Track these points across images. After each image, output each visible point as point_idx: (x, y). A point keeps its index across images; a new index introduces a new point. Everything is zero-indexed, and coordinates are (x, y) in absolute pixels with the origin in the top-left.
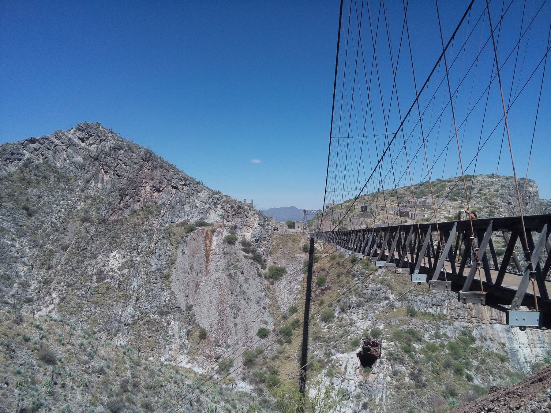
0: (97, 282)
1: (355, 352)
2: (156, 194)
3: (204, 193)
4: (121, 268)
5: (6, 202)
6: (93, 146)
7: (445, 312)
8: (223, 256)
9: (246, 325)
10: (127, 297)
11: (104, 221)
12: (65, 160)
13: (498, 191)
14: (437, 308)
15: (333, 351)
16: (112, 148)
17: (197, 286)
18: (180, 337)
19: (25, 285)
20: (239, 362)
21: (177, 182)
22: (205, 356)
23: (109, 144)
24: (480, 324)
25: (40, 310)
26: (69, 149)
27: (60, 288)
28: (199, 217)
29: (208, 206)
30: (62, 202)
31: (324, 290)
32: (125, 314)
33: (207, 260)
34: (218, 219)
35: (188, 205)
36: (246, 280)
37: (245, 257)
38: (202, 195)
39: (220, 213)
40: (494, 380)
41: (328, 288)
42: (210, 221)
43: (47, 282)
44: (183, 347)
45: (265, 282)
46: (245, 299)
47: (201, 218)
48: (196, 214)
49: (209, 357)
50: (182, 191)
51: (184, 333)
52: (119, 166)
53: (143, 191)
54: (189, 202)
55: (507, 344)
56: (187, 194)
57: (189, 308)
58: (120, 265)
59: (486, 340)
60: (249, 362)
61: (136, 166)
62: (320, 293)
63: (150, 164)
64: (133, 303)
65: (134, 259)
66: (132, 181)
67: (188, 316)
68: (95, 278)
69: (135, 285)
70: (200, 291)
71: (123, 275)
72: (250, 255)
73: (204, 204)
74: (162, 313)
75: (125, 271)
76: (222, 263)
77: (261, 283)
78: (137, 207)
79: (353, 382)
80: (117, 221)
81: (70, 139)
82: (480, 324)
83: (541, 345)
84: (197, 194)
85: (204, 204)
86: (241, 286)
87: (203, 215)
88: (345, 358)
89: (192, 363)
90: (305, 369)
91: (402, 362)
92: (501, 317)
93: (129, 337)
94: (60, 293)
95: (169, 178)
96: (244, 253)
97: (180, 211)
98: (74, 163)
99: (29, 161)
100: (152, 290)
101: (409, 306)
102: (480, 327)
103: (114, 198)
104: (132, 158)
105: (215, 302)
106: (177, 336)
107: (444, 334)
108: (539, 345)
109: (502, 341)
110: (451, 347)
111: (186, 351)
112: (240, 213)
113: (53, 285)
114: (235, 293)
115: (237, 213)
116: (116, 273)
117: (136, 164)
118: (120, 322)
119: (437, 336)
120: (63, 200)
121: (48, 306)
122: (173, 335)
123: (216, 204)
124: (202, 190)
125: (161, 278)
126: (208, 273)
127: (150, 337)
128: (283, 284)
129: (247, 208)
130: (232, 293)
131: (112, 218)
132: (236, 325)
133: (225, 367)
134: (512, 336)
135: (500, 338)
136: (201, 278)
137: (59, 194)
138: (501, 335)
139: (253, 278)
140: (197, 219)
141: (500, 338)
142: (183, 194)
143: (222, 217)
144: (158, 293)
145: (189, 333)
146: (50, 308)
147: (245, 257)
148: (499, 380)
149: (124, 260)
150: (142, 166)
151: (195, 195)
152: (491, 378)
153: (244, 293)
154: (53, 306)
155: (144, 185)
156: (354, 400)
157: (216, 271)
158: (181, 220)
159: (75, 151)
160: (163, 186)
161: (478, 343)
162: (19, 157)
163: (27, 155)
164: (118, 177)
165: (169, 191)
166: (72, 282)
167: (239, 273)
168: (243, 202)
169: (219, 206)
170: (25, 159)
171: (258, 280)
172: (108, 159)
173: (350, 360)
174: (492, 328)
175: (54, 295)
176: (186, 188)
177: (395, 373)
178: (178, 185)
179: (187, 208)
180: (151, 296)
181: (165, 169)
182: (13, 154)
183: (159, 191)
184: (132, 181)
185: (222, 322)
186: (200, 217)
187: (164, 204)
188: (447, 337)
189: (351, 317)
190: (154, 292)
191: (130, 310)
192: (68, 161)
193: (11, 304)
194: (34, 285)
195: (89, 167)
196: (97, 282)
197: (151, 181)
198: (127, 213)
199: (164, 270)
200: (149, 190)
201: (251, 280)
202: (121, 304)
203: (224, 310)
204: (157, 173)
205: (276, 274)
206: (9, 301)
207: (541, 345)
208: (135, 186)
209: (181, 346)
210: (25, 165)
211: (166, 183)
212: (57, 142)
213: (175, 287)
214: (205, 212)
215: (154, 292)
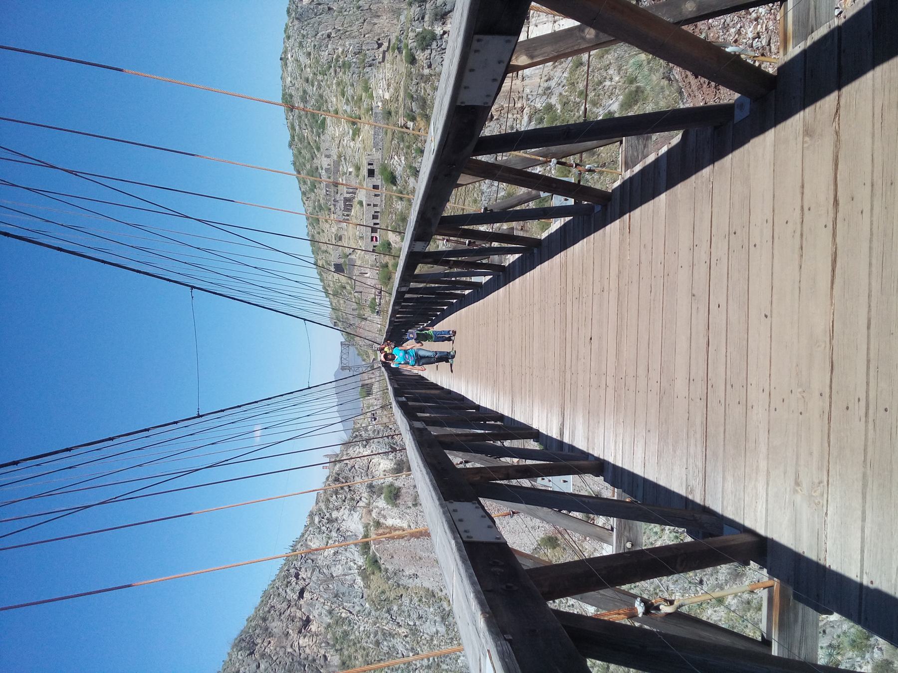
13: (309, 54)
24: (525, 96)
35: (333, 569)
39: (347, 512)
40: (611, 79)
48: (348, 554)
53: (308, 651)
54: (328, 567)
56: (313, 571)
59: (549, 88)
82: (525, 96)
102: (530, 97)
123: (330, 521)
148: (611, 72)
152: (607, 83)
161: (554, 100)
169: (335, 514)
179: (337, 571)
200: (306, 640)
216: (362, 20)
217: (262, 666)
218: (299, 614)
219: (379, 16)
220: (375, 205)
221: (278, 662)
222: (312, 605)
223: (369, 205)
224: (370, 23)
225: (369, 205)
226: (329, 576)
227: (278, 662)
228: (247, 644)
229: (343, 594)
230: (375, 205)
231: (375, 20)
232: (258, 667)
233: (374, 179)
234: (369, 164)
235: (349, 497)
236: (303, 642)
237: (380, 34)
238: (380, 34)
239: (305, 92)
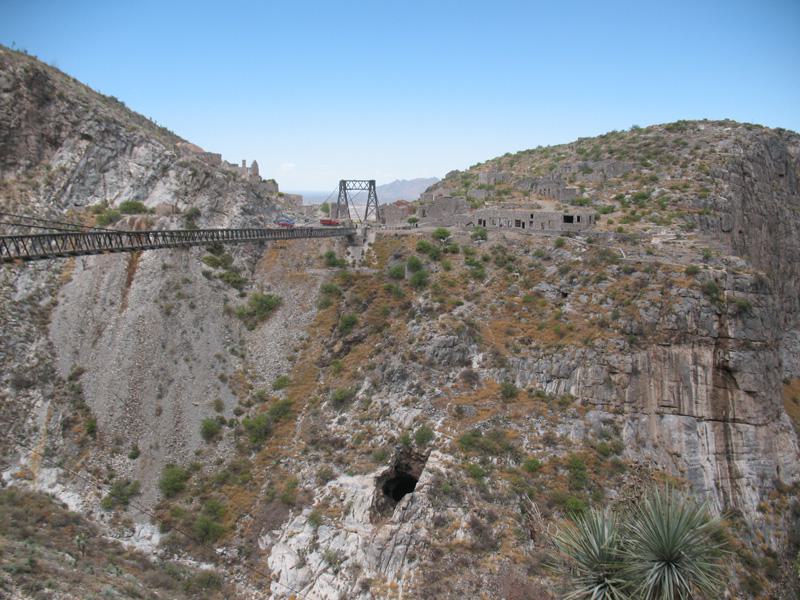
1: (373, 475)
7: (573, 391)
9: (178, 411)
13: (726, 151)
14: (559, 384)
15: (336, 470)
17: (99, 333)
24: (637, 416)
29: (151, 173)
31: (350, 343)
33: (129, 284)
34: (168, 198)
35: (112, 171)
36: (196, 322)
37: (207, 274)
39: (174, 188)
41: (358, 340)
42: (149, 204)
44: (49, 453)
46: (187, 360)
47: (137, 197)
48: (127, 189)
50: (101, 144)
53: (23, 145)
54: (115, 167)
55: (685, 455)
56: (112, 150)
57: (77, 374)
60: (173, 487)
62: (341, 351)
70: (103, 343)
72: (221, 271)
73: (143, 168)
77: (227, 327)
79: (354, 535)
82: (637, 416)
83: (751, 456)
84: (132, 150)
85: (143, 168)
86: (184, 332)
87: (140, 192)
88: (353, 485)
89: (63, 484)
91: (457, 497)
92: (679, 400)
96: (205, 267)
101: (507, 380)
102: (636, 421)
105: (127, 363)
107: (563, 437)
108: (746, 456)
109: (676, 448)
110: (574, 466)
112: (208, 186)
115: (203, 186)
119: (549, 441)
122: (36, 429)
123: (165, 169)
128: (272, 328)
130: (164, 347)
132: (159, 412)
133: (122, 496)
134: (696, 438)
135: (672, 442)
138: (675, 435)
141: (672, 442)
144: (19, 345)
145: (67, 425)
147: (207, 274)
151: (128, 151)
156: (347, 574)
157: (141, 302)
158: (97, 202)
160: (63, 134)
169: (172, 173)
171: (222, 320)
173: (360, 487)
174: (660, 423)
177: (439, 522)
179: (110, 177)
185: (132, 406)
186: (135, 194)
188: (570, 444)
189: (387, 401)
190: (11, 343)
197: (37, 125)
199: (40, 299)
200: (34, 143)
203: (141, 381)
207: (751, 456)
216: (765, 212)
217: (6, 95)
218: (63, 134)
219: (770, 232)
220: (531, 222)
221: (11, 112)
222: (73, 149)
223: (532, 216)
224: (762, 221)
225: (532, 216)
226: (107, 167)
227: (11, 112)
228: (40, 83)
229: (83, 184)
230: (531, 222)
231: (765, 228)
232: (6, 91)
233: (561, 222)
234: (579, 218)
235: (189, 189)
236: (33, 139)
237: (747, 233)
238: (747, 233)
239: (685, 144)
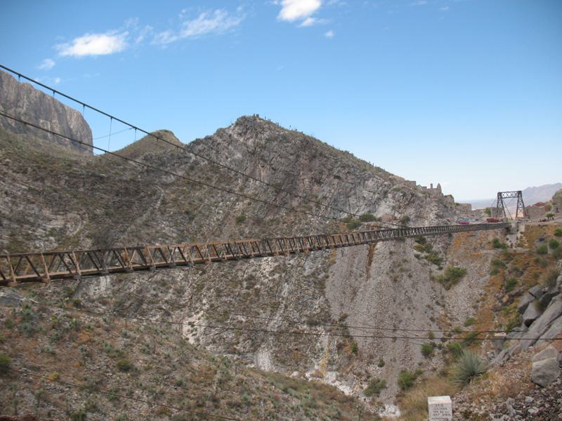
0: (247, 288)
2: (316, 187)
3: (373, 180)
4: (272, 273)
5: (170, 207)
6: (251, 140)
8: (388, 257)
10: (275, 307)
11: (258, 221)
12: (227, 158)
16: (268, 140)
17: (355, 293)
18: (330, 351)
19: (180, 292)
20: (394, 388)
21: (339, 171)
22: (355, 374)
23: (266, 135)
25: (191, 316)
26: (230, 147)
27: (210, 294)
28: (366, 210)
29: (377, 196)
30: (221, 204)
31: (513, 296)
32: (272, 323)
33: (370, 263)
34: (388, 211)
35: (354, 197)
36: (413, 285)
37: (417, 256)
38: (370, 183)
39: (392, 204)
42: (378, 215)
43: (200, 288)
44: (331, 363)
45: (438, 286)
47: (369, 212)
48: (363, 206)
49: (359, 375)
50: (346, 181)
51: (333, 347)
52: (274, 159)
54: (355, 194)
56: (352, 184)
57: (344, 318)
58: (271, 269)
61: (291, 157)
62: (508, 301)
63: (307, 153)
64: (282, 312)
65: (287, 262)
66: (287, 174)
67: (341, 327)
68: (245, 284)
69: (285, 293)
71: (274, 280)
72: (424, 254)
73: (372, 194)
74: (312, 323)
75: (277, 276)
76: (387, 264)
78: (295, 203)
80: (272, 221)
81: (230, 136)
84: (364, 183)
85: (372, 194)
87: (371, 208)
89: (340, 381)
90: (347, 400)
93: (274, 348)
94: (210, 299)
95: (330, 167)
96: (415, 252)
97: (344, 205)
98: (234, 160)
99: (196, 163)
100: (303, 297)
103: (270, 196)
104: (287, 149)
105: (373, 311)
106: (326, 348)
111: (334, 367)
112: (413, 202)
113: (204, 291)
114: (398, 301)
116: (267, 278)
117: (292, 154)
118: (266, 331)
120: (222, 201)
121: (198, 313)
122: (322, 349)
123: (386, 193)
124: (370, 177)
125: (315, 283)
126: (368, 277)
127: (297, 349)
128: (461, 288)
129: (420, 195)
130: (394, 301)
131: (268, 219)
133: (376, 388)
136: (360, 283)
137: (219, 195)
139: (423, 282)
140: (363, 212)
142: (347, 185)
143: (394, 208)
145: (340, 347)
146: (199, 315)
147: (417, 256)
149: (276, 264)
150: (298, 156)
151: (362, 183)
153: (409, 300)
154: (202, 312)
155: (302, 178)
159: (235, 148)
162: (185, 160)
163: (194, 158)
164: (273, 172)
165: (331, 182)
166: (221, 288)
167: (405, 277)
168: (429, 187)
169: (390, 195)
170: (191, 161)
172: (265, 153)
175: (204, 301)
176: (350, 177)
178: (341, 175)
179: (352, 200)
180: (302, 304)
181: (325, 157)
182: (179, 158)
183: (319, 182)
184: (287, 174)
187: (325, 198)
191: (277, 318)
192: (229, 159)
193: (164, 310)
194: (188, 291)
195: (247, 164)
196: (247, 288)
197: (309, 173)
198: (283, 212)
199: (319, 274)
201: (420, 285)
202: (269, 313)
204: (316, 163)
205: (455, 277)
206: (163, 307)
208: (291, 178)
209: (329, 361)
210: (192, 168)
211: (327, 173)
212: (219, 140)
213: (329, 293)
214: (375, 204)
215: (305, 300)
